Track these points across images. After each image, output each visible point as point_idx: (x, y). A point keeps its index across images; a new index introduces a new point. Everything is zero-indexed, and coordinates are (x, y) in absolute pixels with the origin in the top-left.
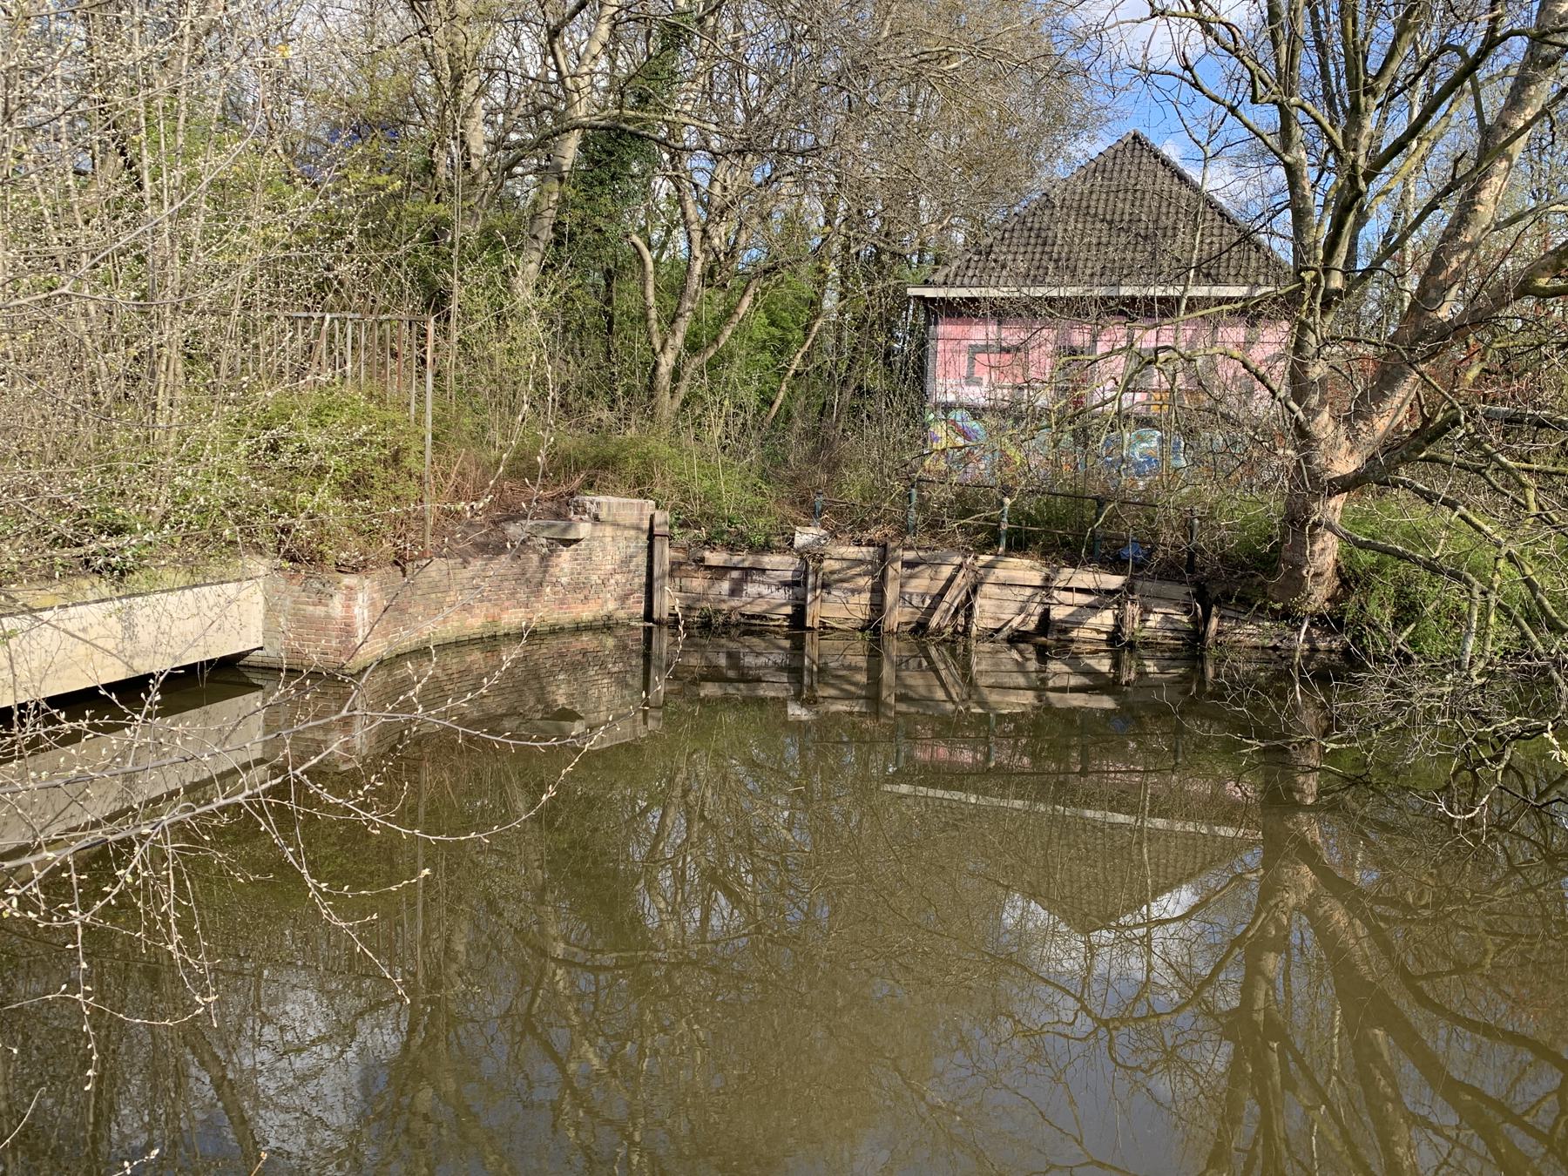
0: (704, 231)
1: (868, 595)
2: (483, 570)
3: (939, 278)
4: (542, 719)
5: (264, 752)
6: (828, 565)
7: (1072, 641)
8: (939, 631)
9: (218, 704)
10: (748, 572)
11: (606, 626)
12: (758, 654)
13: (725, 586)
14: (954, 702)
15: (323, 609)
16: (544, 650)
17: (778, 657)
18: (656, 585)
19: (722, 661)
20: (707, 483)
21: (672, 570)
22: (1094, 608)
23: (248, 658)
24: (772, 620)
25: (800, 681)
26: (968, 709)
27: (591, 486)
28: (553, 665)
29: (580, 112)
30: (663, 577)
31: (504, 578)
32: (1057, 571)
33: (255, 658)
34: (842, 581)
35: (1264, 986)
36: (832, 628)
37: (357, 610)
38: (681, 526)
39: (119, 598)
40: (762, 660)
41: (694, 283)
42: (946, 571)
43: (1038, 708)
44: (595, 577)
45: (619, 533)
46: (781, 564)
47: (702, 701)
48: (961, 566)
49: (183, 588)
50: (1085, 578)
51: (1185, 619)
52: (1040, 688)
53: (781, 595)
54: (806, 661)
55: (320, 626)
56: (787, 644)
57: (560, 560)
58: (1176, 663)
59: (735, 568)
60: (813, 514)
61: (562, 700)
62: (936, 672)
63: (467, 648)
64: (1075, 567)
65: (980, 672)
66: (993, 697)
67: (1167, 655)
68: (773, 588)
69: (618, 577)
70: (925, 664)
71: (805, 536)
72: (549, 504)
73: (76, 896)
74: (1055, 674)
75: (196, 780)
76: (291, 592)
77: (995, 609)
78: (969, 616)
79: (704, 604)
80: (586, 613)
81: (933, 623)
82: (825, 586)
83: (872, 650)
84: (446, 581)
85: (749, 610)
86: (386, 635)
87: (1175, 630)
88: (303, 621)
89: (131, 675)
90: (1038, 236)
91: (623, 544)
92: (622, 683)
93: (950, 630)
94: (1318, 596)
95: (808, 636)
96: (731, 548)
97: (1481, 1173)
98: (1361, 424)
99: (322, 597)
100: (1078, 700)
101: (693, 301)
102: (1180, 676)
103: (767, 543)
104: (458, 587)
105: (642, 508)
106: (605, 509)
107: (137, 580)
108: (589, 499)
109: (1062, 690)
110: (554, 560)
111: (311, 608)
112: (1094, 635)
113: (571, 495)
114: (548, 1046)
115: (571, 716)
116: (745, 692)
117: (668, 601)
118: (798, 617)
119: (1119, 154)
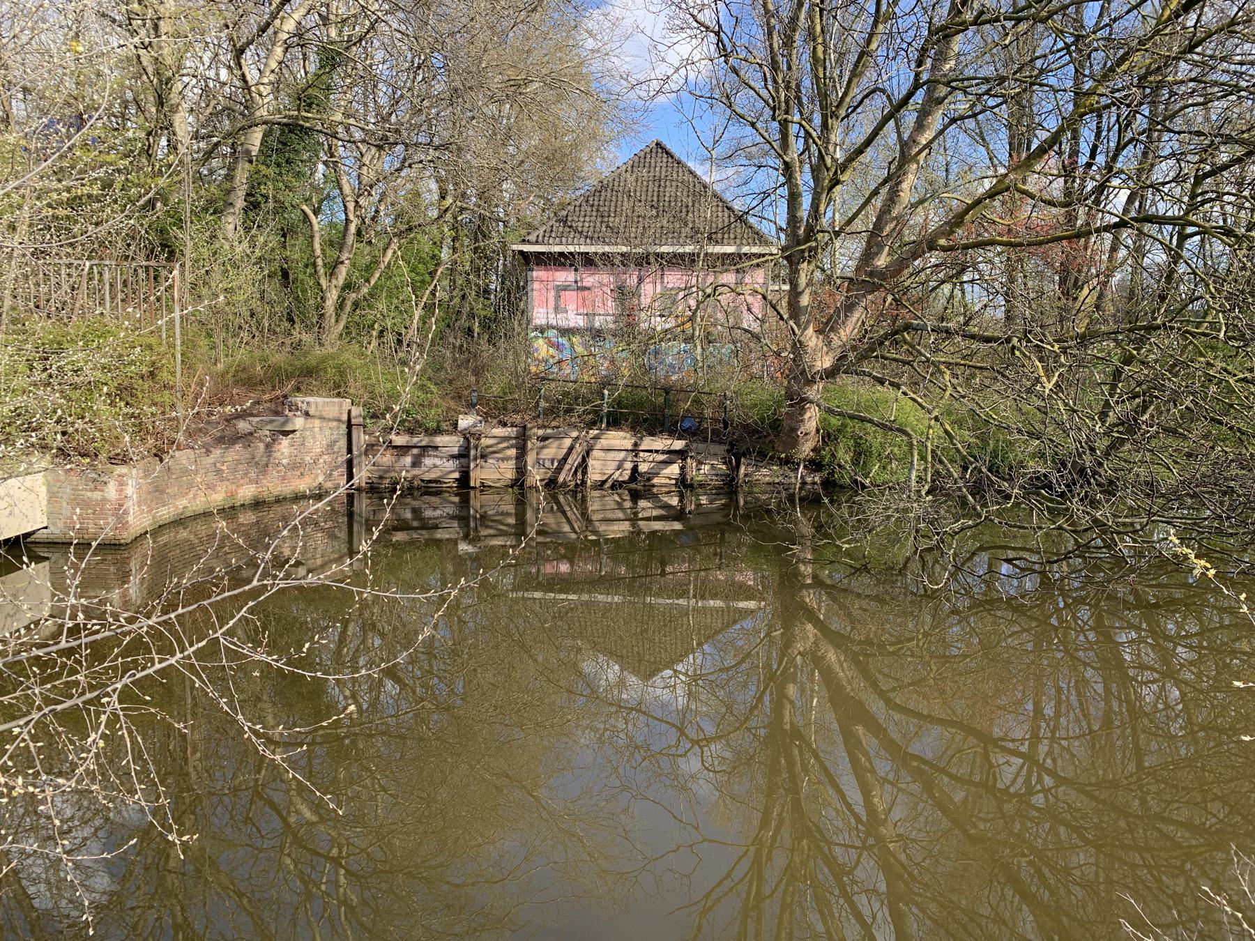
0: (357, 202)
2: (222, 457)
3: (532, 238)
6: (485, 442)
7: (653, 486)
8: (565, 484)
9: (12, 575)
10: (424, 449)
12: (435, 508)
13: (408, 460)
14: (576, 532)
15: (100, 493)
16: (271, 515)
17: (450, 510)
19: (408, 515)
20: (389, 385)
21: (366, 450)
22: (667, 463)
23: (35, 536)
25: (468, 525)
26: (586, 537)
27: (298, 389)
29: (263, 113)
30: (360, 455)
31: (238, 462)
32: (641, 439)
34: (494, 452)
35: (788, 706)
36: (490, 486)
38: (372, 417)
40: (438, 513)
41: (351, 238)
42: (567, 442)
43: (632, 533)
44: (308, 458)
46: (450, 443)
48: (577, 438)
50: (660, 443)
51: (724, 467)
52: (634, 519)
53: (451, 465)
54: (472, 512)
56: (456, 499)
57: (281, 446)
58: (721, 497)
60: (471, 406)
62: (564, 513)
64: (653, 435)
65: (593, 511)
66: (602, 528)
67: (714, 491)
68: (445, 460)
69: (326, 457)
70: (555, 508)
71: (465, 422)
72: (268, 405)
73: (37, 762)
74: (643, 509)
77: (599, 468)
78: (584, 473)
79: (393, 474)
80: (303, 485)
81: (561, 479)
82: (483, 456)
83: (518, 500)
85: (427, 477)
87: (717, 475)
90: (598, 211)
91: (328, 432)
92: (333, 537)
93: (573, 483)
94: (806, 449)
95: (472, 493)
96: (411, 432)
98: (832, 335)
99: (98, 484)
100: (658, 526)
101: (350, 252)
102: (723, 505)
103: (438, 426)
104: (203, 471)
105: (341, 405)
106: (313, 407)
108: (299, 399)
109: (648, 519)
110: (276, 447)
111: (89, 494)
112: (667, 481)
113: (285, 397)
114: (271, 803)
116: (427, 537)
117: (362, 475)
118: (464, 480)
119: (648, 156)
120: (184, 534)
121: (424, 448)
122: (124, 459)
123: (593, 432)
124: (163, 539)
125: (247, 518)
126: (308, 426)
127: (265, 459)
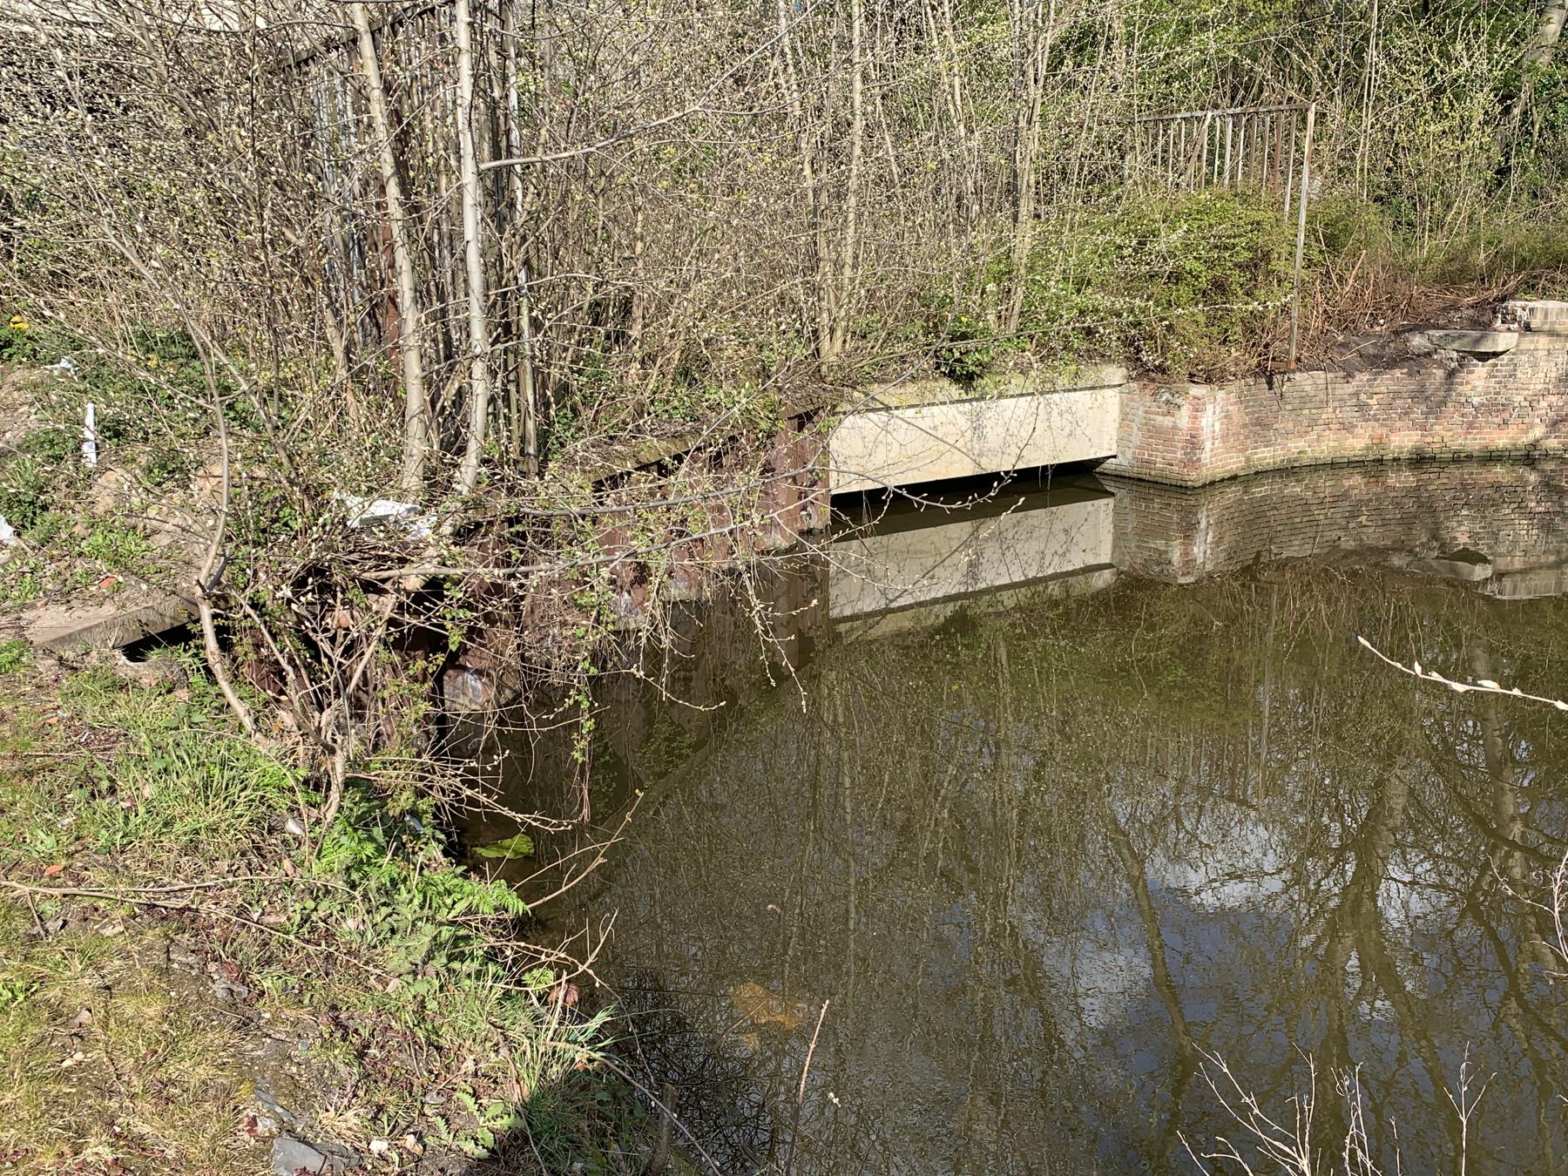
4: (1437, 558)
5: (1112, 557)
9: (1065, 507)
11: (1529, 457)
15: (1171, 419)
16: (1439, 483)
28: (1454, 498)
31: (1397, 395)
33: (1109, 465)
37: (1204, 422)
55: (1164, 436)
61: (1463, 540)
63: (1344, 472)
69: (1553, 399)
72: (1471, 312)
75: (1040, 575)
76: (1143, 401)
80: (1501, 440)
84: (1322, 396)
86: (1243, 451)
88: (1153, 431)
89: (978, 472)
97: (788, 1172)
99: (1172, 408)
110: (1462, 376)
111: (1160, 418)
113: (1504, 299)
115: (1476, 558)
120: (1294, 488)
122: (1211, 376)
124: (1259, 491)
125: (1403, 479)
126: (1523, 346)
127: (1442, 393)
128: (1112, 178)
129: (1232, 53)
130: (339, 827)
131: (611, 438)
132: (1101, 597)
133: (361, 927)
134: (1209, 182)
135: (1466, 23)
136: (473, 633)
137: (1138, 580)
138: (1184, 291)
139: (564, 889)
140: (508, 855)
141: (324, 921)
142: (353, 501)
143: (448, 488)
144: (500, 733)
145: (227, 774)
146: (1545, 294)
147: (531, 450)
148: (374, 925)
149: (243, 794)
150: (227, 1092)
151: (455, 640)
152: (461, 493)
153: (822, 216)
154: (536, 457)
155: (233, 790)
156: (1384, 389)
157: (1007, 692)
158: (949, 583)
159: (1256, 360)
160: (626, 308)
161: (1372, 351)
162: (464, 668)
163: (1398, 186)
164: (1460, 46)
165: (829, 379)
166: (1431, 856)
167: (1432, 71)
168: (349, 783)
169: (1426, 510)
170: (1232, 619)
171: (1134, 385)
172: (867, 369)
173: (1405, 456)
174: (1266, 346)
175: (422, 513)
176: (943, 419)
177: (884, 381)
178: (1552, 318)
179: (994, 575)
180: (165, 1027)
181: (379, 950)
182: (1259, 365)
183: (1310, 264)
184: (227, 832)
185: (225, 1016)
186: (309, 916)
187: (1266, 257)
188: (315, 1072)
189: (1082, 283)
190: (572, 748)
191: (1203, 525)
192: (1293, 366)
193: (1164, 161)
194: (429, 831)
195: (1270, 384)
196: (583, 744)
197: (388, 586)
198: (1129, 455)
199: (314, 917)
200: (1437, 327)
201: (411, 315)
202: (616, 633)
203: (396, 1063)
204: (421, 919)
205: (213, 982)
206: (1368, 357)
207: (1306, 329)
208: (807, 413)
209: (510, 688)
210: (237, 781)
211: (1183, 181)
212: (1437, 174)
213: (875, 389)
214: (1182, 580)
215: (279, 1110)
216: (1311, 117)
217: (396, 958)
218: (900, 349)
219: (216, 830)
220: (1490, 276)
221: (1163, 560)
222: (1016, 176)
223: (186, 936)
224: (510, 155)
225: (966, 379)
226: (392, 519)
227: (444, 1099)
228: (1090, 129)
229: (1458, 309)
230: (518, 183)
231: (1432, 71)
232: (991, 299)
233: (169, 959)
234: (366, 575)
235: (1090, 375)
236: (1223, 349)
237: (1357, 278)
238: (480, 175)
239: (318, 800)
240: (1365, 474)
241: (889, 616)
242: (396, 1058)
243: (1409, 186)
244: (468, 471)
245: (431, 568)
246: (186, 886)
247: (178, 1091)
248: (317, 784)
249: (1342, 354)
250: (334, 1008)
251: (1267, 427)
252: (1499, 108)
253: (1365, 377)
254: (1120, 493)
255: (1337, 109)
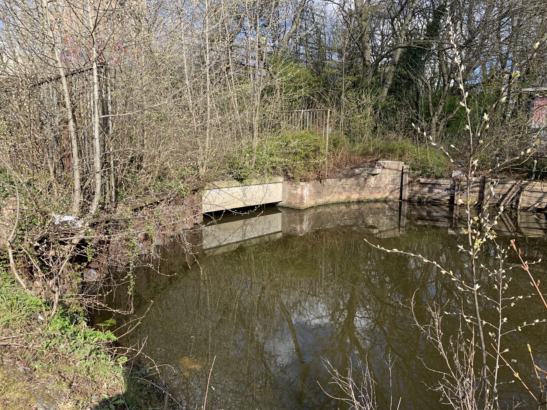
1: (478, 194)
11: (385, 201)
12: (437, 212)
13: (426, 189)
14: (510, 232)
16: (363, 207)
17: (444, 214)
18: (403, 188)
19: (424, 214)
20: (423, 157)
24: (443, 201)
25: (452, 221)
28: (368, 212)
30: (406, 185)
33: (280, 204)
38: (413, 170)
39: (242, 186)
40: (439, 214)
42: (508, 186)
45: (391, 172)
47: (418, 226)
49: (259, 184)
53: (446, 193)
55: (294, 196)
56: (448, 209)
59: (429, 184)
69: (391, 186)
72: (370, 163)
76: (288, 186)
80: (378, 196)
84: (334, 185)
85: (435, 197)
88: (291, 194)
92: (391, 219)
95: (455, 207)
105: (399, 164)
106: (386, 164)
107: (246, 181)
113: (377, 160)
115: (374, 227)
117: (406, 194)
120: (328, 210)
121: (433, 184)
122: (306, 180)
123: (524, 182)
124: (319, 210)
125: (355, 207)
128: (278, 127)
129: (308, 95)
130: (56, 317)
131: (137, 197)
132: (279, 241)
133: (66, 347)
134: (303, 128)
135: (365, 90)
136: (95, 256)
137: (288, 235)
138: (298, 157)
139: (128, 332)
140: (108, 325)
141: (54, 346)
142: (57, 217)
143: (88, 211)
144: (104, 287)
145: (19, 302)
146: (387, 159)
147: (113, 200)
148: (71, 346)
149: (24, 308)
150: (27, 401)
151: (90, 258)
152: (92, 213)
153: (199, 134)
154: (115, 202)
155: (21, 307)
156: (349, 183)
157: (253, 268)
158: (236, 238)
159: (317, 176)
160: (141, 159)
161: (346, 173)
162: (90, 268)
163: (350, 131)
164: (364, 96)
165: (202, 180)
166: (367, 309)
167: (357, 102)
168: (59, 303)
169: (361, 215)
170: (313, 246)
171: (286, 182)
172: (213, 177)
173: (355, 201)
174: (319, 172)
175: (79, 220)
176: (235, 191)
177: (218, 181)
178: (389, 165)
179: (250, 235)
180: (4, 382)
181: (72, 353)
182: (318, 177)
183: (329, 151)
184: (19, 320)
185: (23, 377)
186: (48, 345)
187: (319, 148)
188: (56, 392)
189: (271, 155)
190: (128, 291)
191: (305, 220)
192: (326, 177)
193: (291, 122)
194: (82, 318)
195: (321, 182)
196: (131, 289)
197: (68, 242)
198: (285, 201)
199: (50, 345)
200: (362, 167)
201: (76, 160)
202: (139, 255)
203: (82, 387)
204: (86, 343)
205: (18, 367)
206: (345, 175)
207: (329, 168)
208: (196, 189)
209: (105, 273)
210: (22, 304)
211: (297, 128)
212: (360, 128)
213: (216, 183)
214: (300, 235)
215: (44, 405)
216: (329, 112)
217: (79, 355)
218: (223, 172)
219: (15, 320)
220: (374, 154)
221: (295, 230)
222: (252, 126)
223: (8, 353)
224: (108, 114)
225: (241, 180)
226: (69, 221)
227: (98, 397)
228: (272, 114)
229: (366, 163)
230: (110, 122)
231: (357, 102)
232: (247, 158)
233: (2, 361)
234: (61, 239)
235: (274, 179)
236: (308, 173)
237: (341, 155)
238: (100, 119)
239: (49, 308)
240: (346, 206)
241: (220, 248)
242: (82, 386)
243: (353, 131)
244: (94, 208)
245: (82, 236)
246: (6, 338)
247: (9, 402)
248: (49, 303)
249: (338, 174)
250: (59, 372)
251: (320, 193)
252: (374, 112)
253: (344, 180)
254: (283, 212)
255: (334, 111)
